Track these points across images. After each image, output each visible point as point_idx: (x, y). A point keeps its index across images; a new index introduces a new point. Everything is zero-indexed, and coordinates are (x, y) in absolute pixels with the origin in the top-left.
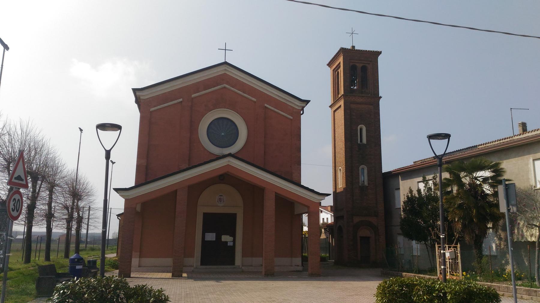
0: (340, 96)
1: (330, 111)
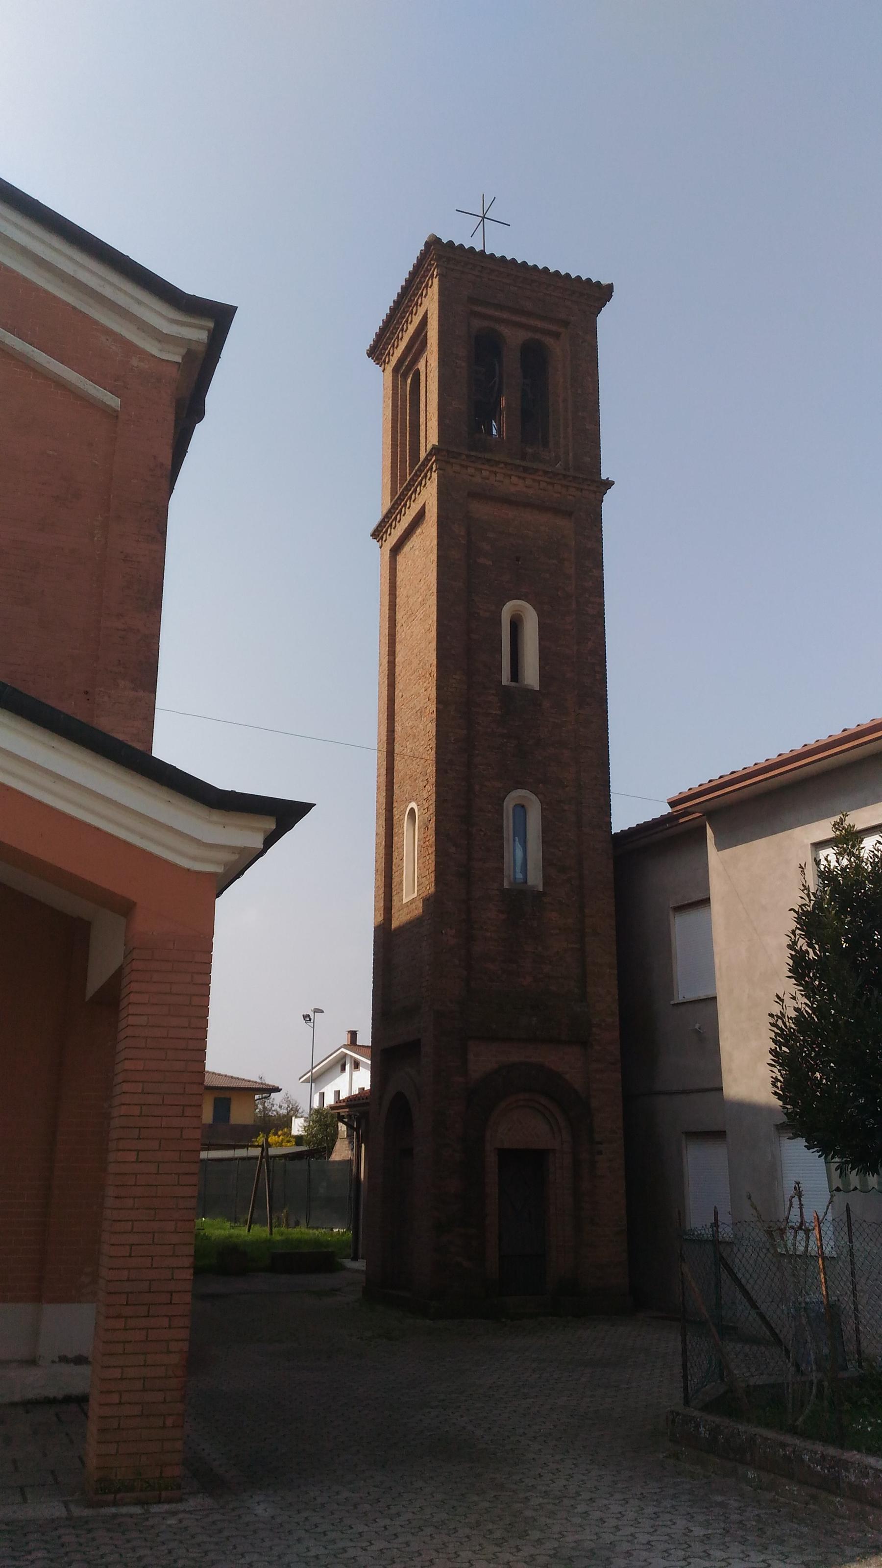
0: (423, 455)
1: (375, 555)
